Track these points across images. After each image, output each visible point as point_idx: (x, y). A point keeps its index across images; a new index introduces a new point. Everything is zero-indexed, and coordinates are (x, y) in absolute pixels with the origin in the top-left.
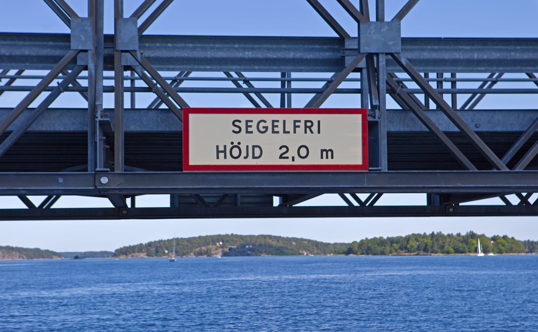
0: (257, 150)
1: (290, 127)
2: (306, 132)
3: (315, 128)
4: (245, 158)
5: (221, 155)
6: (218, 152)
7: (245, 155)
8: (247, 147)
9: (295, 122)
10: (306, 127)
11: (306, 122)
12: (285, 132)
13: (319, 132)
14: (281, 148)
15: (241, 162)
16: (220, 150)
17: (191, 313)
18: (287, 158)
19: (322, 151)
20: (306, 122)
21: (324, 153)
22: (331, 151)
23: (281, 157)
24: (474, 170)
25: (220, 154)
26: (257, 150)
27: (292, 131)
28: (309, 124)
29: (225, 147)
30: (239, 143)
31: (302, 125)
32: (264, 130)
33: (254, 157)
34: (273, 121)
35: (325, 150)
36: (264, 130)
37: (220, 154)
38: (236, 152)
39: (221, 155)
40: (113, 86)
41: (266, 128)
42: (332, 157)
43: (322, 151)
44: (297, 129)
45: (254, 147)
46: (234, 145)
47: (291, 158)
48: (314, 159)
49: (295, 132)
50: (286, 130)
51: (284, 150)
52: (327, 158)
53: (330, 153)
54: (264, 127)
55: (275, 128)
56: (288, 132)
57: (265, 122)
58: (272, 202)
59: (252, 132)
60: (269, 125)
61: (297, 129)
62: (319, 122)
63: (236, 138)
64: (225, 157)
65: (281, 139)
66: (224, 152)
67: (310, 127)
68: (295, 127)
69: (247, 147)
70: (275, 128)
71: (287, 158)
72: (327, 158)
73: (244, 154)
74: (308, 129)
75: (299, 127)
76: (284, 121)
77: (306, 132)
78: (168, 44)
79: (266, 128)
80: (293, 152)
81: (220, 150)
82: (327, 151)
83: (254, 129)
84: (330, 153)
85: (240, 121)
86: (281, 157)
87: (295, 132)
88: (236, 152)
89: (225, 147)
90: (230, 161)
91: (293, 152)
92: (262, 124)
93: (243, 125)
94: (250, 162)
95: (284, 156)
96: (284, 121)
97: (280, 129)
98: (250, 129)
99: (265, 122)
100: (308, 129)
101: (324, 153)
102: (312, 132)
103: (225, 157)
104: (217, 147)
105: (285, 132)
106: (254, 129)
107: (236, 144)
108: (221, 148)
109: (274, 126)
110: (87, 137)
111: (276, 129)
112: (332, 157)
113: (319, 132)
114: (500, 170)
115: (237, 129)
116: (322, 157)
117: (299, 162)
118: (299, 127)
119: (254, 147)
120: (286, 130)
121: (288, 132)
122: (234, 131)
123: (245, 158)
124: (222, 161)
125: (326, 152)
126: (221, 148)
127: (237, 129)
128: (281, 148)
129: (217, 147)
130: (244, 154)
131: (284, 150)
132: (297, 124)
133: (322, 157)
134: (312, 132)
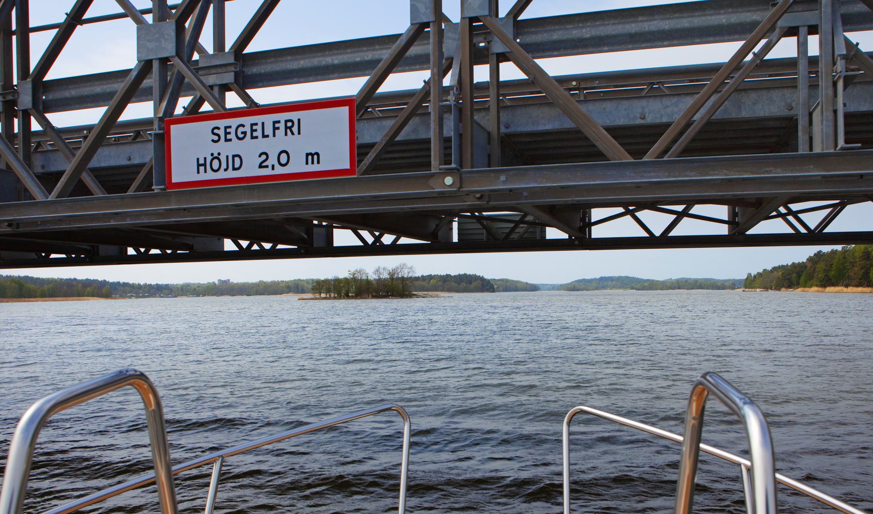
0: (237, 160)
1: (269, 130)
2: (286, 134)
3: (295, 129)
4: (226, 170)
5: (202, 169)
6: (199, 165)
7: (225, 167)
8: (227, 157)
9: (275, 123)
10: (286, 128)
11: (286, 121)
12: (264, 136)
13: (299, 133)
14: (260, 156)
15: (221, 175)
16: (200, 163)
17: (712, 362)
18: (267, 167)
19: (307, 155)
20: (286, 121)
21: (310, 157)
22: (317, 154)
23: (261, 166)
24: (627, 159)
25: (200, 168)
26: (237, 160)
27: (271, 135)
28: (289, 124)
29: (205, 159)
30: (219, 154)
31: (282, 126)
32: (243, 135)
33: (234, 169)
34: (252, 125)
35: (311, 154)
36: (243, 135)
37: (200, 168)
38: (215, 166)
39: (202, 169)
40: (488, 82)
41: (245, 133)
42: (318, 162)
43: (307, 155)
44: (276, 131)
45: (234, 156)
46: (214, 156)
47: (270, 167)
48: (297, 166)
49: (274, 135)
50: (265, 134)
51: (264, 157)
52: (313, 163)
53: (316, 157)
54: (242, 133)
55: (228, 135)
56: (267, 136)
57: (243, 126)
58: (316, 220)
59: (230, 140)
60: (247, 129)
61: (276, 131)
62: (299, 120)
63: (216, 149)
64: (205, 172)
65: (262, 145)
66: (205, 165)
67: (290, 128)
68: (275, 129)
69: (227, 157)
70: (228, 135)
71: (267, 167)
72: (313, 163)
73: (224, 166)
74: (288, 130)
75: (278, 128)
76: (263, 124)
77: (286, 134)
78: (638, 18)
79: (245, 133)
80: (272, 160)
81: (200, 163)
82: (312, 155)
83: (232, 136)
84: (316, 157)
85: (218, 128)
86: (261, 166)
87: (274, 135)
88: (215, 166)
89: (205, 159)
90: (210, 176)
91: (272, 160)
92: (241, 129)
93: (221, 132)
94: (231, 174)
95: (263, 164)
96: (263, 124)
97: (259, 133)
98: (229, 137)
99: (243, 126)
100: (288, 130)
101: (310, 157)
102: (293, 134)
103: (205, 172)
104: (198, 159)
105: (264, 136)
106: (232, 136)
107: (216, 155)
108: (202, 161)
109: (253, 131)
110: (429, 149)
111: (255, 134)
112: (318, 162)
113: (299, 133)
114: (62, 173)
115: (216, 138)
116: (307, 163)
117: (279, 170)
118: (278, 128)
119: (234, 156)
120: (265, 134)
121: (267, 136)
122: (213, 141)
123: (226, 170)
124: (203, 177)
125: (313, 156)
126: (202, 161)
127: (216, 138)
128: (260, 156)
129: (198, 159)
130: (224, 166)
131: (264, 157)
132: (277, 125)
133: (307, 163)
134: (293, 134)
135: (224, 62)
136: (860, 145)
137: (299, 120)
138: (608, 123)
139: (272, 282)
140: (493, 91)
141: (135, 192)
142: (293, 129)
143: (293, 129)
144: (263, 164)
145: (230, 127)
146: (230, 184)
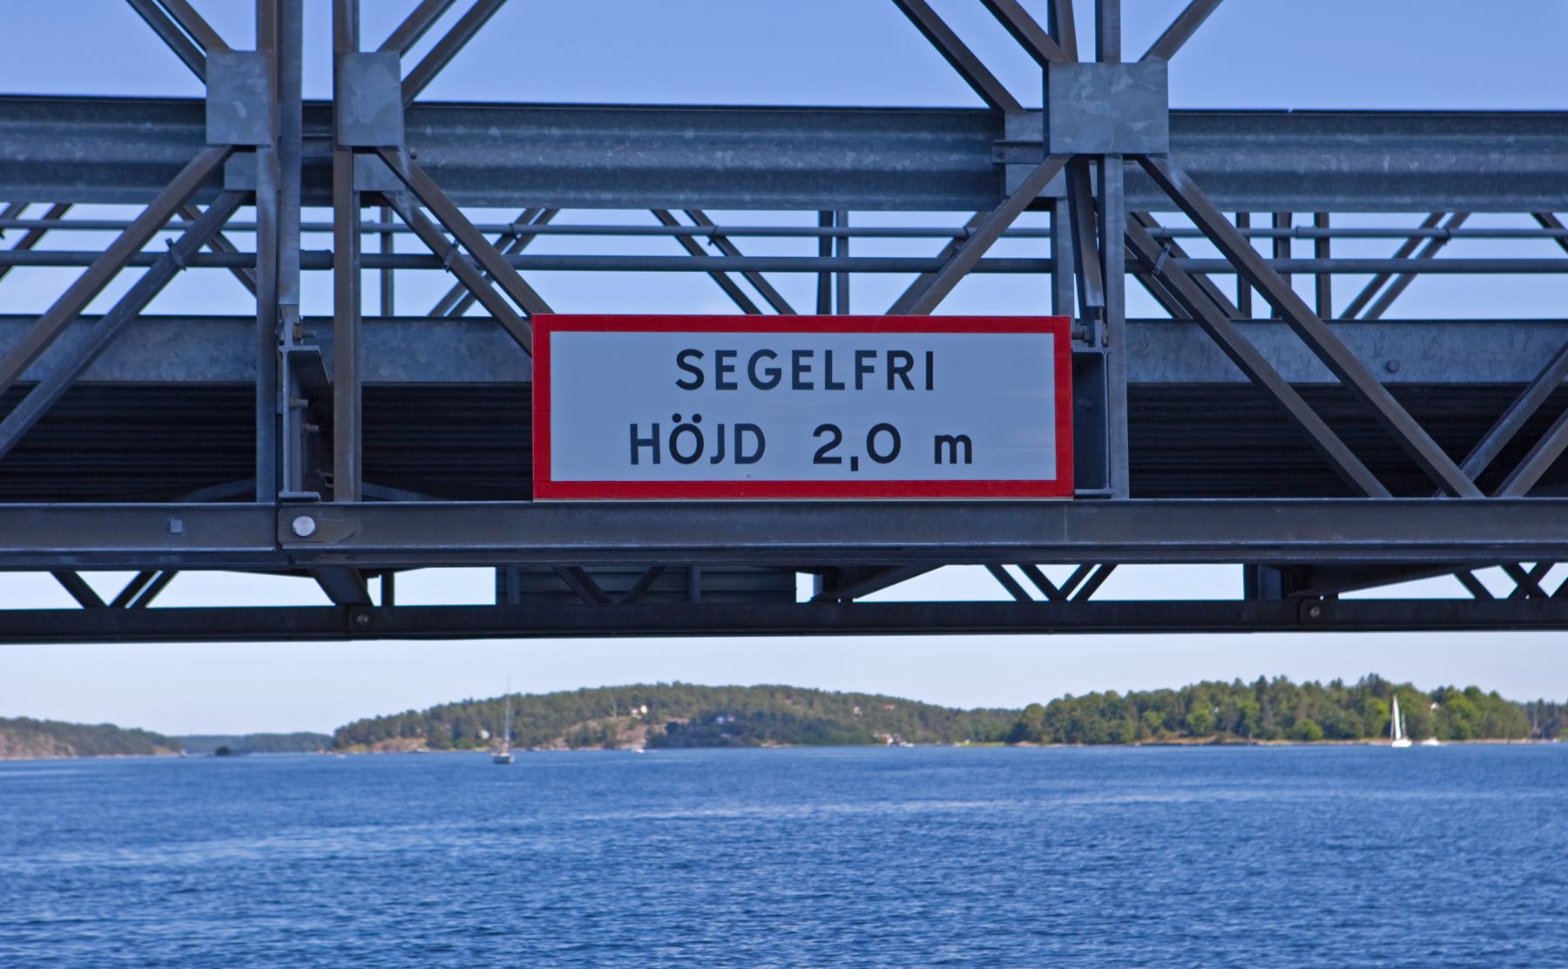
0: (749, 439)
1: (844, 371)
2: (891, 386)
3: (917, 375)
4: (715, 460)
5: (645, 452)
6: (636, 443)
7: (715, 454)
8: (721, 428)
10: (892, 370)
11: (892, 355)
12: (830, 385)
13: (929, 386)
14: (818, 432)
15: (701, 472)
18: (837, 460)
19: (939, 440)
20: (892, 355)
21: (946, 446)
22: (966, 440)
23: (819, 458)
24: (1381, 496)
26: (749, 439)
27: (850, 382)
28: (900, 362)
29: (656, 428)
30: (697, 418)
31: (880, 363)
32: (770, 378)
33: (740, 459)
35: (948, 438)
36: (770, 378)
38: (686, 444)
39: (645, 452)
41: (776, 373)
42: (968, 460)
43: (939, 440)
44: (865, 376)
45: (740, 428)
46: (682, 422)
47: (847, 462)
48: (915, 465)
49: (859, 386)
50: (835, 380)
51: (828, 437)
52: (953, 460)
53: (961, 446)
54: (768, 371)
56: (841, 386)
57: (772, 355)
59: (733, 386)
60: (785, 364)
61: (865, 376)
62: (930, 356)
63: (688, 404)
64: (657, 459)
65: (820, 405)
66: (654, 442)
67: (903, 372)
68: (861, 370)
69: (721, 428)
71: (837, 460)
72: (953, 460)
73: (711, 449)
74: (897, 377)
75: (870, 369)
76: (829, 354)
77: (891, 386)
79: (776, 373)
80: (853, 445)
82: (953, 442)
83: (739, 375)
84: (961, 446)
85: (699, 355)
86: (819, 458)
87: (859, 386)
88: (686, 444)
89: (656, 428)
90: (670, 471)
91: (853, 445)
92: (763, 363)
93: (708, 366)
94: (730, 471)
95: (827, 455)
96: (829, 354)
97: (816, 376)
99: (772, 355)
100: (897, 377)
101: (946, 446)
102: (909, 386)
103: (657, 459)
104: (634, 428)
105: (830, 385)
106: (739, 375)
107: (687, 419)
108: (645, 433)
109: (797, 369)
110: (254, 399)
111: (804, 377)
112: (968, 460)
113: (929, 386)
115: (691, 378)
116: (938, 460)
117: (870, 472)
118: (870, 369)
119: (740, 428)
120: (835, 380)
121: (841, 386)
122: (681, 384)
123: (715, 460)
124: (646, 471)
125: (951, 444)
126: (645, 433)
127: (691, 378)
128: (818, 432)
129: (634, 428)
130: (711, 449)
131: (828, 437)
132: (866, 362)
133: (938, 460)
134: (909, 386)
135: (1199, 289)
136: (128, 606)
137: (930, 356)
138: (1293, 378)
139: (1157, 692)
140: (842, 229)
141: (1526, 496)
142: (908, 374)
143: (908, 374)
144: (827, 455)
145: (733, 354)
146: (723, 497)
